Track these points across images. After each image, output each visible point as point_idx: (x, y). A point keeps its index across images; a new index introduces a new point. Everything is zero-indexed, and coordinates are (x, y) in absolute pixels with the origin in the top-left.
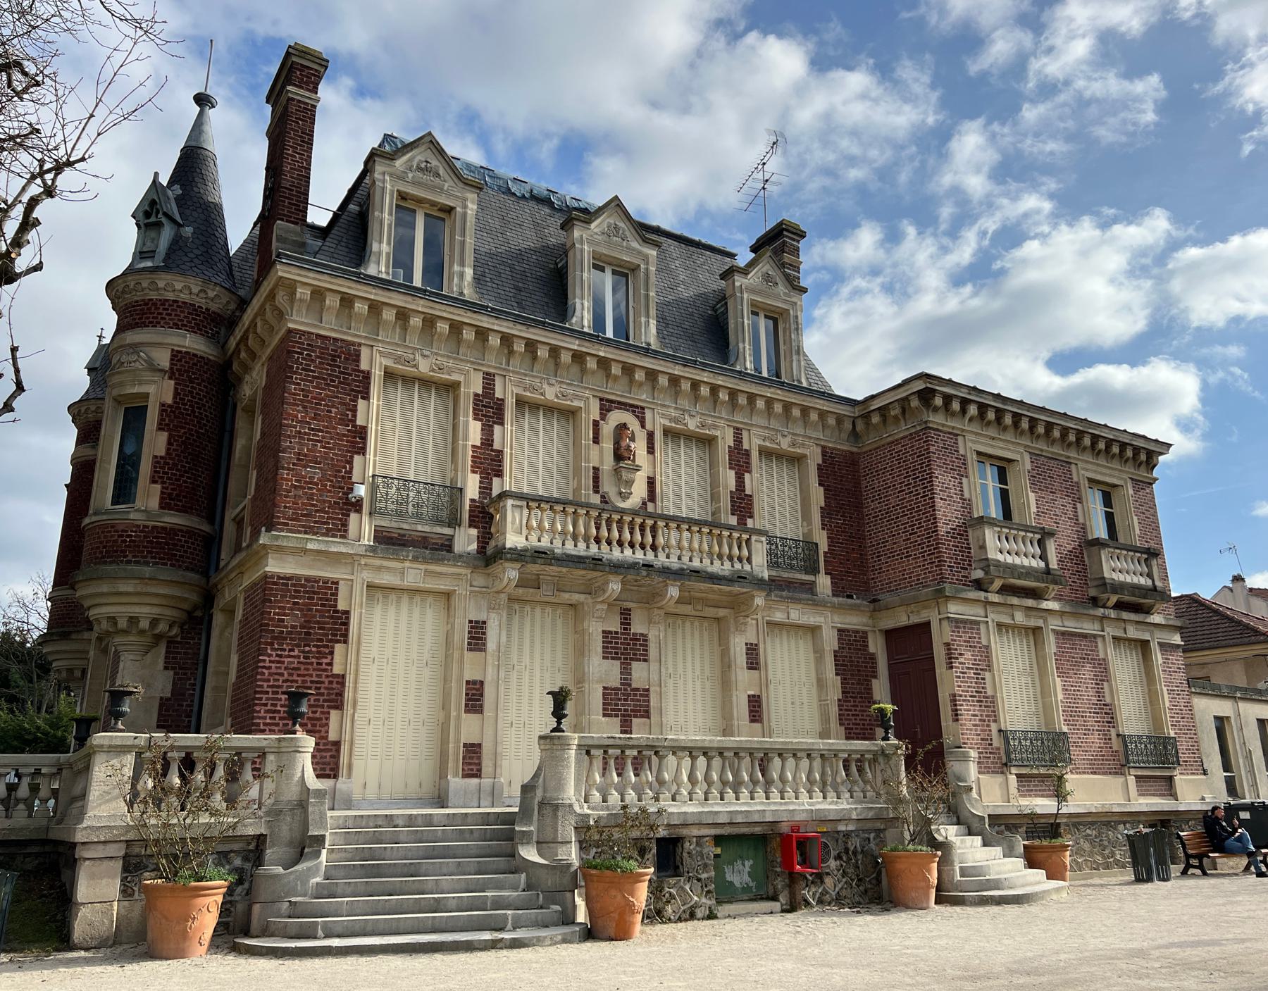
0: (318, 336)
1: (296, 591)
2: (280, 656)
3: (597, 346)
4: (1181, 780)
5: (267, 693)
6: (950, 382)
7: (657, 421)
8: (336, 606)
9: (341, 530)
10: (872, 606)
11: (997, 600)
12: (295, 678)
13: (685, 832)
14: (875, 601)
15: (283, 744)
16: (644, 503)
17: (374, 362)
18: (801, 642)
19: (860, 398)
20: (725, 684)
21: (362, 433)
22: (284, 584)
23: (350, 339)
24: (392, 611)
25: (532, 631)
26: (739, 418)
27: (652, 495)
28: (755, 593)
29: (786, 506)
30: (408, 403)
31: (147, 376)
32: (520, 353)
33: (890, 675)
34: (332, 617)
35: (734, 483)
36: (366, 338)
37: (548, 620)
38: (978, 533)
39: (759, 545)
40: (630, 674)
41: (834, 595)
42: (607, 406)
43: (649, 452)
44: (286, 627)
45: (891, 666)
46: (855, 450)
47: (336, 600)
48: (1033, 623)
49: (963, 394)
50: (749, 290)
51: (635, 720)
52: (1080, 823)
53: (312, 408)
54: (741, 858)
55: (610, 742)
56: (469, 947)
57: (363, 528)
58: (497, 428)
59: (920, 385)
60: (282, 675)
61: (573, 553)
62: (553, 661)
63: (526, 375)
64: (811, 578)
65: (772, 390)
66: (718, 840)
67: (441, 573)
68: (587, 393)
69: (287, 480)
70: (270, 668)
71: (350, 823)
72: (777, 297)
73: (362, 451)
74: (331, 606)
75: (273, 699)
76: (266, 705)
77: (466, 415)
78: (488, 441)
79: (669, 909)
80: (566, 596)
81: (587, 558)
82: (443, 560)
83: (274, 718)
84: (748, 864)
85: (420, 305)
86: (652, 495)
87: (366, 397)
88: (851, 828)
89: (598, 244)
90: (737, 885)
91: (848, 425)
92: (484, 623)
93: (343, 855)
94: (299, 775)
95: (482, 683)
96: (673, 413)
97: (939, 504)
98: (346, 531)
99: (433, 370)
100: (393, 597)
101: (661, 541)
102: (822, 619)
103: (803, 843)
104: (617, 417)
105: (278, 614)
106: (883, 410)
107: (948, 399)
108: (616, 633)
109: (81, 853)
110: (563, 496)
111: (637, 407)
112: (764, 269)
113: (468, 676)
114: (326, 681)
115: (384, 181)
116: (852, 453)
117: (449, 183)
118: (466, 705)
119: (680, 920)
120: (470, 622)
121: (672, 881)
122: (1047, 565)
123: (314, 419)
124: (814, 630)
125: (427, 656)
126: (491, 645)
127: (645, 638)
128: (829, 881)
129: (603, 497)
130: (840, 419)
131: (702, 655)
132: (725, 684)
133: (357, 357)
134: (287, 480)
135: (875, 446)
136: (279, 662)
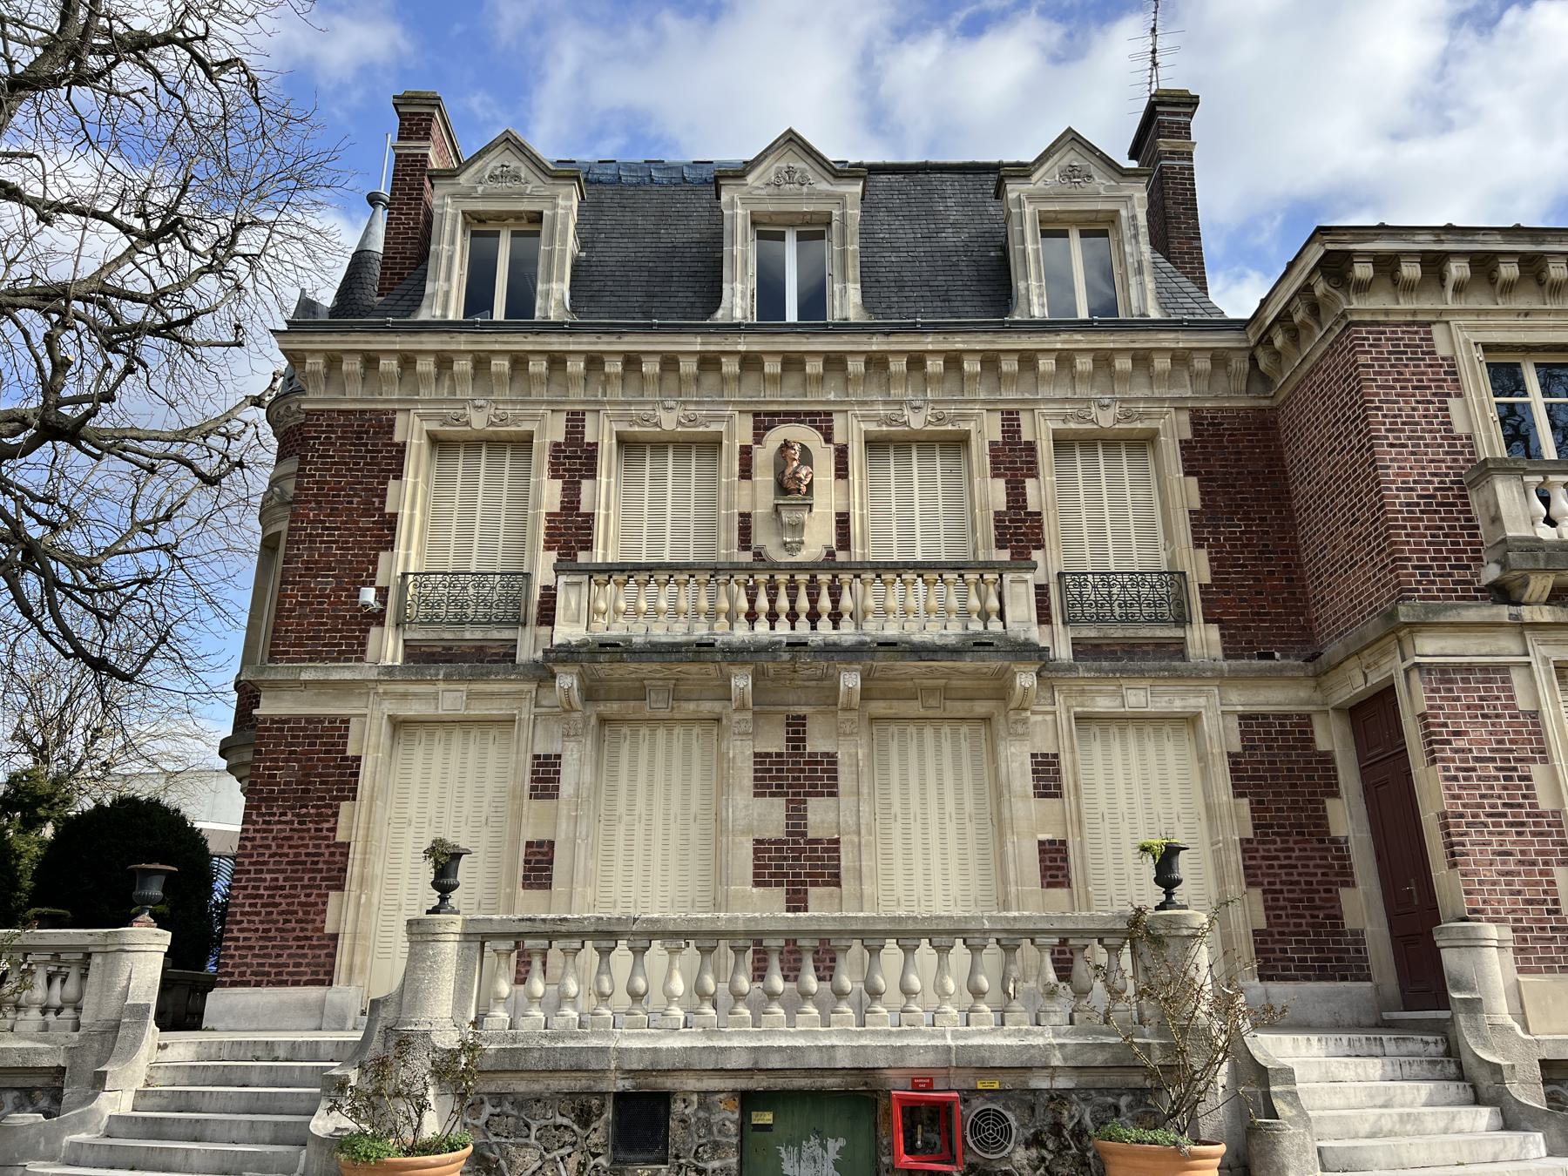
0: (340, 412)
1: (293, 737)
2: (268, 823)
3: (731, 339)
5: (249, 872)
6: (1383, 230)
7: (852, 429)
8: (344, 751)
9: (355, 650)
10: (1310, 667)
12: (286, 850)
13: (668, 1083)
14: (1313, 658)
15: (109, 941)
16: (831, 554)
17: (412, 431)
19: (1248, 316)
21: (391, 522)
22: (278, 729)
23: (380, 406)
25: (651, 762)
27: (844, 541)
28: (1015, 667)
29: (1126, 522)
32: (616, 375)
33: (1366, 789)
34: (339, 767)
35: (1004, 498)
36: (399, 401)
37: (677, 747)
38: (1486, 494)
39: (1021, 588)
40: (805, 817)
41: (1227, 657)
42: (763, 423)
43: (838, 477)
44: (278, 784)
45: (1365, 770)
46: (1265, 403)
47: (345, 744)
50: (1031, 198)
51: (812, 891)
53: (328, 502)
54: (818, 1133)
55: (525, 927)
57: (387, 646)
58: (586, 485)
59: (1316, 253)
60: (269, 847)
61: (664, 640)
62: (685, 806)
63: (630, 403)
64: (1179, 633)
65: (1064, 336)
66: (749, 1100)
67: (492, 694)
69: (291, 596)
70: (254, 839)
71: (225, 1053)
72: (1096, 196)
73: (390, 545)
74: (338, 752)
75: (255, 880)
76: (245, 888)
78: (571, 501)
80: (692, 706)
81: (688, 644)
82: (488, 674)
83: (254, 905)
84: (834, 1146)
85: (462, 342)
86: (844, 541)
87: (398, 477)
88: (1062, 1083)
89: (760, 200)
91: (1240, 364)
92: (559, 757)
93: (157, 1101)
94: (124, 983)
95: (551, 844)
96: (881, 410)
97: (1386, 454)
98: (364, 652)
99: (493, 424)
101: (846, 602)
102: (1202, 701)
103: (939, 1114)
104: (775, 438)
105: (269, 768)
106: (1284, 317)
107: (1387, 265)
108: (779, 755)
110: (680, 559)
111: (818, 414)
112: (1065, 162)
113: (529, 835)
114: (327, 852)
116: (1261, 410)
117: (533, 182)
118: (525, 878)
120: (537, 757)
123: (329, 515)
124: (1191, 720)
125: (486, 810)
126: (566, 787)
127: (831, 759)
130: (1219, 359)
131: (958, 778)
132: (999, 825)
133: (391, 426)
134: (291, 596)
135: (1291, 387)
136: (265, 831)
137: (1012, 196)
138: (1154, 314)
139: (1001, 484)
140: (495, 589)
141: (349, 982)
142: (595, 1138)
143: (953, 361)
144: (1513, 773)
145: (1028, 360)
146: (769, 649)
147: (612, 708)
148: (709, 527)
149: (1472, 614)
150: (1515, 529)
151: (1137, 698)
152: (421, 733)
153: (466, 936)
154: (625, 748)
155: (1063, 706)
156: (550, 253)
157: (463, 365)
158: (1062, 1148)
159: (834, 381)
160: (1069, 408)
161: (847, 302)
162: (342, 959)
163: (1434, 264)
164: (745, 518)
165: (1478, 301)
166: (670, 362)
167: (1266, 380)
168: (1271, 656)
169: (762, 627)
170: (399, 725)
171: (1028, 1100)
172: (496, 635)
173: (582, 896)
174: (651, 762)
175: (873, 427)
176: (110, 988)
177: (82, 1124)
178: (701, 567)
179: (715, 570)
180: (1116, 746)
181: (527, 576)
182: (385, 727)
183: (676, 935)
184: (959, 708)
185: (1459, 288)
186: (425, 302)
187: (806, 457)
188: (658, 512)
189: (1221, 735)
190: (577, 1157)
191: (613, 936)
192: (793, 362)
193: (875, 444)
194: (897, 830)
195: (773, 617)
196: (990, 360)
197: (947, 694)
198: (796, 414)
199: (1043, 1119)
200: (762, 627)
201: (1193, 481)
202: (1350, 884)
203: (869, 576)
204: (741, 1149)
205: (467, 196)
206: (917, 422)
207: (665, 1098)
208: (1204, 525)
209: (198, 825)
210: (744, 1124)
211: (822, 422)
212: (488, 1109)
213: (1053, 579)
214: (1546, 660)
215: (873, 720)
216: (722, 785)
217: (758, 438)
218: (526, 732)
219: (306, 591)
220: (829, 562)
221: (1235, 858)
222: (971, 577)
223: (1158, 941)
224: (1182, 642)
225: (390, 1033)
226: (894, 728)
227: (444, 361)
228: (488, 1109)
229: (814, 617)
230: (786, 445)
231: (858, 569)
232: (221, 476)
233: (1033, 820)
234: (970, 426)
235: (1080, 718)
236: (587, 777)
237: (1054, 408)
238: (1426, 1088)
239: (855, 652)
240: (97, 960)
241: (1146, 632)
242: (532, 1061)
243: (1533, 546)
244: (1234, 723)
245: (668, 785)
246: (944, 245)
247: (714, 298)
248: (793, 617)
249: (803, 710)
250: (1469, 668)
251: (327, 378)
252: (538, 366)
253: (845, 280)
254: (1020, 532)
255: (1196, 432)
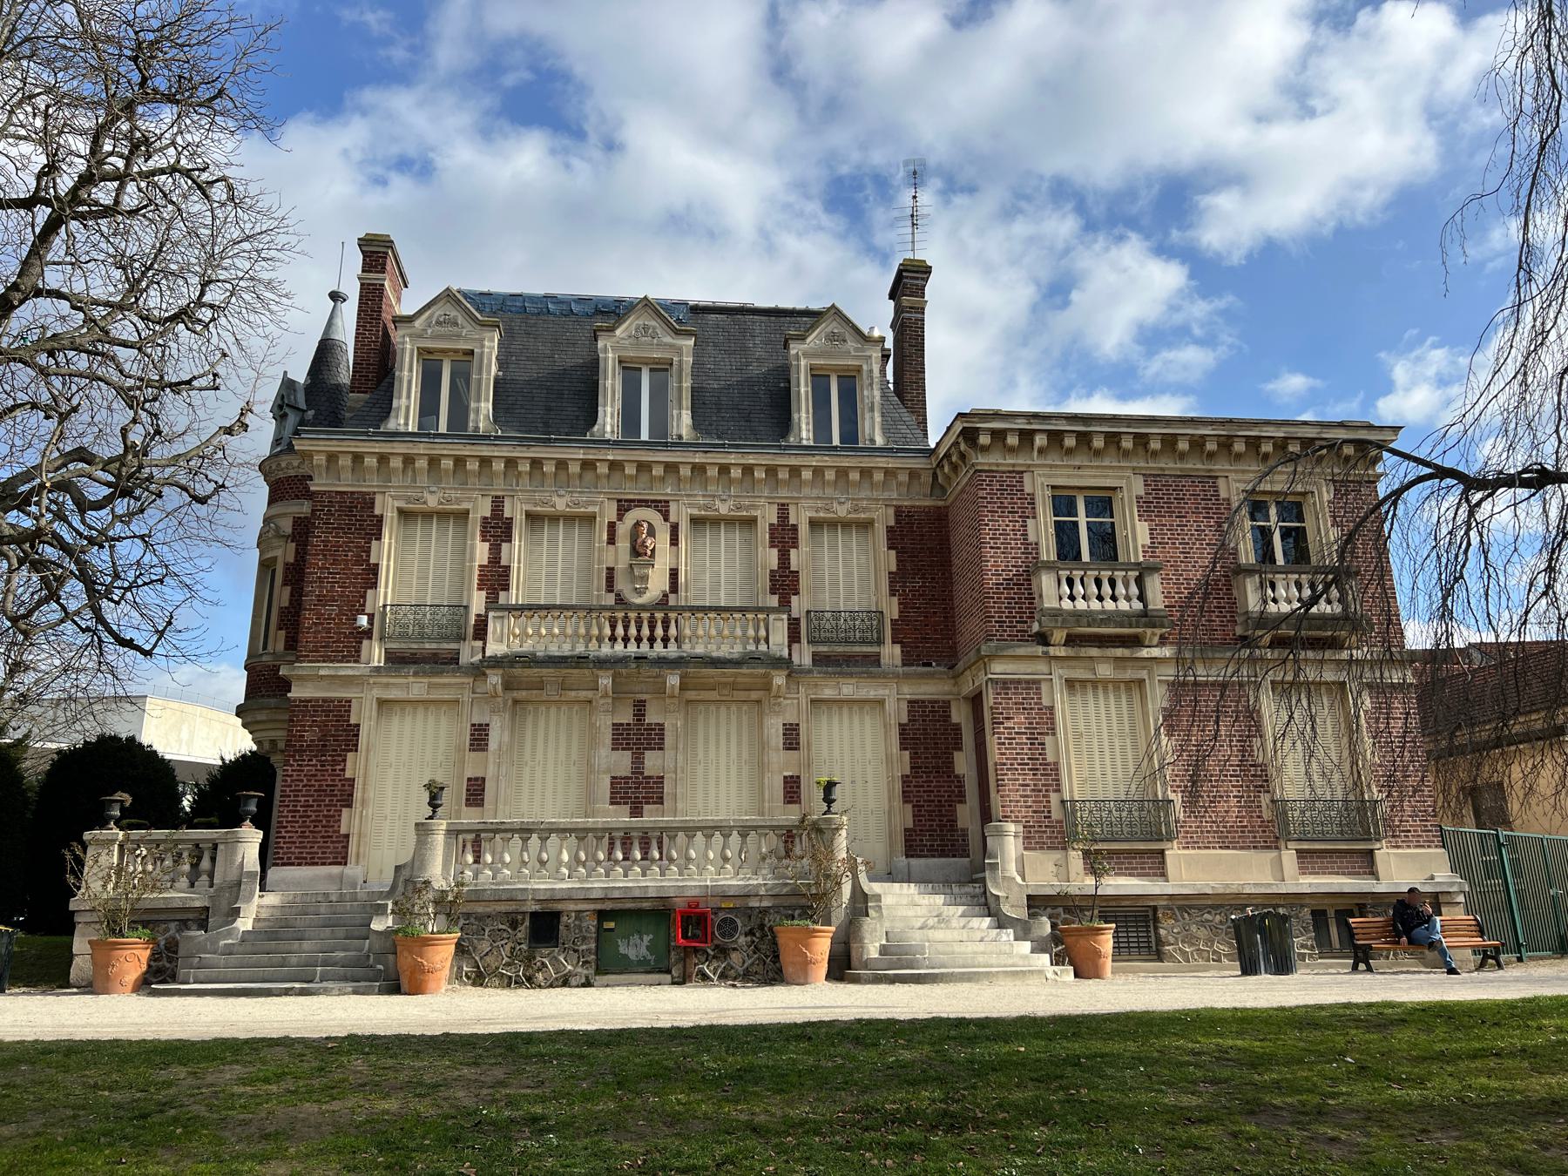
4: (1385, 854)
7: (681, 513)
9: (355, 656)
11: (1063, 654)
13: (559, 907)
16: (666, 595)
17: (387, 507)
18: (867, 719)
20: (761, 767)
21: (374, 570)
24: (408, 719)
25: (547, 729)
26: (783, 493)
27: (674, 586)
29: (850, 577)
30: (427, 537)
31: (276, 542)
35: (486, 555)
37: (563, 718)
39: (779, 624)
42: (624, 507)
46: (941, 503)
48: (1129, 674)
49: (1021, 424)
52: (1191, 907)
56: (268, 993)
57: (375, 654)
59: (958, 427)
62: (568, 755)
66: (602, 915)
68: (601, 498)
73: (374, 585)
77: (473, 539)
79: (540, 976)
80: (573, 693)
84: (646, 938)
85: (421, 449)
86: (674, 586)
87: (379, 539)
88: (765, 904)
89: (625, 348)
90: (633, 957)
91: (927, 478)
100: (409, 709)
109: (77, 918)
112: (829, 329)
113: (469, 773)
115: (404, 343)
119: (551, 986)
121: (546, 951)
122: (1145, 606)
124: (880, 703)
125: (441, 758)
126: (493, 744)
127: (661, 727)
128: (735, 958)
129: (618, 595)
130: (913, 474)
131: (739, 735)
132: (761, 767)
137: (793, 352)
138: (879, 441)
139: (775, 552)
140: (444, 616)
141: (357, 863)
142: (519, 935)
143: (748, 470)
144: (1036, 743)
145: (795, 471)
146: (622, 661)
147: (522, 695)
148: (586, 573)
149: (1021, 651)
150: (1050, 602)
151: (848, 689)
152: (397, 708)
153: (449, 832)
154: (530, 718)
155: (803, 694)
156: (480, 381)
157: (422, 464)
158: (764, 935)
159: (671, 479)
160: (820, 504)
161: (683, 423)
162: (352, 849)
163: (1027, 436)
164: (610, 570)
165: (1053, 459)
166: (562, 464)
167: (943, 489)
168: (930, 665)
169: (619, 647)
170: (382, 703)
171: (748, 912)
172: (445, 646)
173: (502, 808)
174: (547, 729)
175: (695, 512)
176: (232, 862)
177: (229, 934)
178: (581, 608)
179: (590, 610)
180: (836, 719)
181: (466, 607)
182: (375, 706)
183: (564, 830)
184: (742, 695)
185: (1041, 451)
186: (393, 414)
187: (652, 532)
188: (552, 563)
189: (897, 712)
190: (510, 944)
191: (530, 831)
192: (643, 467)
193: (696, 521)
194: (700, 770)
195: (626, 640)
196: (771, 471)
197: (734, 687)
198: (646, 501)
199: (754, 922)
200: (619, 647)
201: (893, 553)
202: (963, 802)
203: (687, 614)
204: (597, 941)
205: (420, 336)
206: (724, 509)
207: (556, 915)
208: (897, 581)
209: (167, 757)
210: (599, 927)
211: (662, 507)
212: (462, 922)
213: (803, 614)
214: (1061, 677)
215: (688, 702)
216: (592, 743)
217: (620, 517)
218: (467, 709)
219: (319, 615)
220: (662, 603)
221: (898, 786)
222: (750, 616)
223: (820, 831)
224: (878, 654)
225: (408, 881)
226: (701, 707)
227: (409, 460)
228: (462, 922)
229: (652, 640)
230: (638, 524)
231: (680, 609)
232: (209, 497)
233: (781, 763)
234: (758, 513)
235: (812, 701)
236: (506, 738)
237: (811, 503)
238: (961, 909)
239: (678, 663)
240: (221, 847)
241: (857, 649)
242: (486, 896)
243: (1057, 614)
244: (904, 706)
245: (557, 739)
246: (751, 375)
247: (592, 418)
248: (639, 640)
249: (643, 697)
250: (1019, 682)
251: (328, 468)
252: (473, 466)
253: (680, 408)
254: (785, 583)
255: (897, 521)
